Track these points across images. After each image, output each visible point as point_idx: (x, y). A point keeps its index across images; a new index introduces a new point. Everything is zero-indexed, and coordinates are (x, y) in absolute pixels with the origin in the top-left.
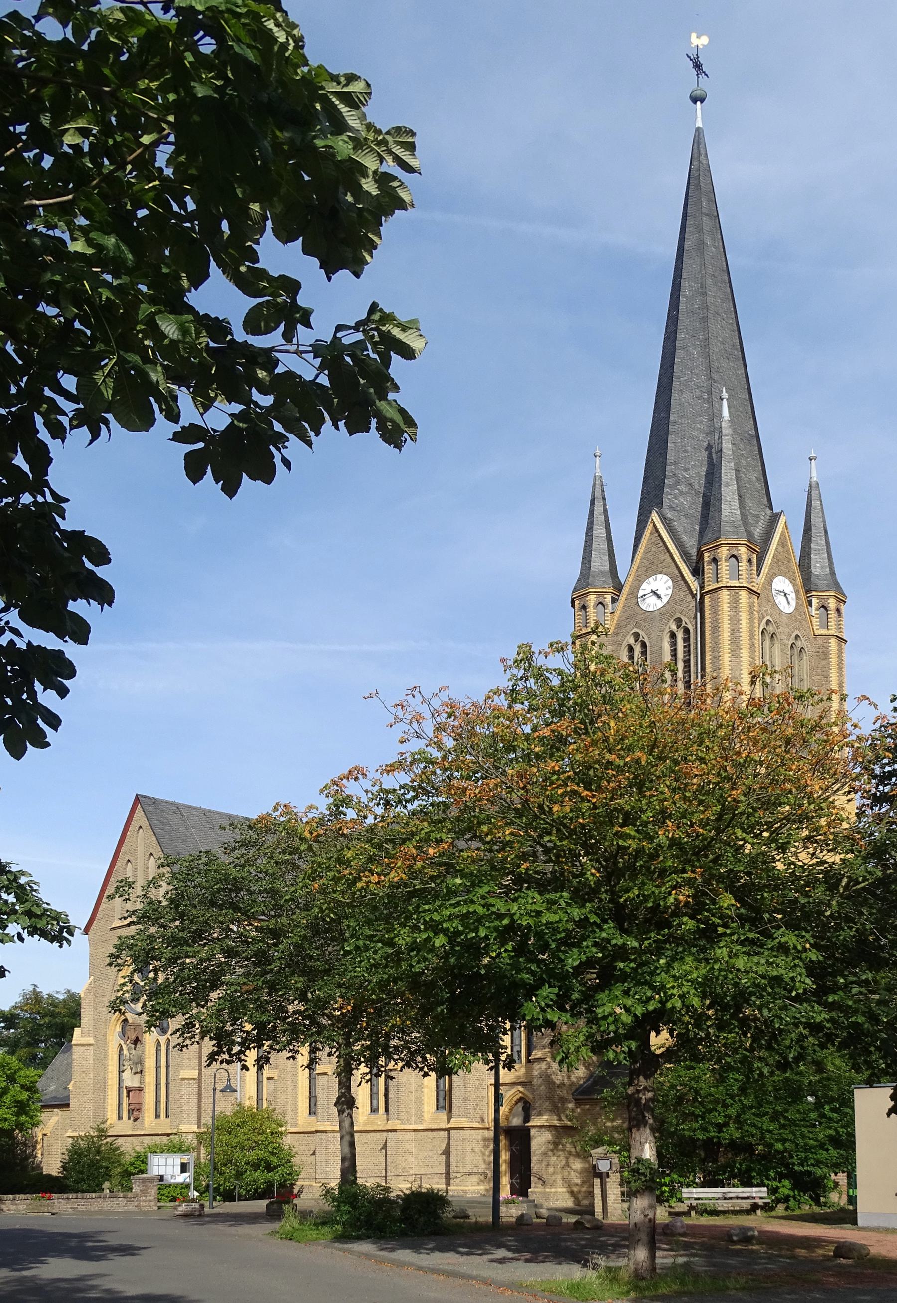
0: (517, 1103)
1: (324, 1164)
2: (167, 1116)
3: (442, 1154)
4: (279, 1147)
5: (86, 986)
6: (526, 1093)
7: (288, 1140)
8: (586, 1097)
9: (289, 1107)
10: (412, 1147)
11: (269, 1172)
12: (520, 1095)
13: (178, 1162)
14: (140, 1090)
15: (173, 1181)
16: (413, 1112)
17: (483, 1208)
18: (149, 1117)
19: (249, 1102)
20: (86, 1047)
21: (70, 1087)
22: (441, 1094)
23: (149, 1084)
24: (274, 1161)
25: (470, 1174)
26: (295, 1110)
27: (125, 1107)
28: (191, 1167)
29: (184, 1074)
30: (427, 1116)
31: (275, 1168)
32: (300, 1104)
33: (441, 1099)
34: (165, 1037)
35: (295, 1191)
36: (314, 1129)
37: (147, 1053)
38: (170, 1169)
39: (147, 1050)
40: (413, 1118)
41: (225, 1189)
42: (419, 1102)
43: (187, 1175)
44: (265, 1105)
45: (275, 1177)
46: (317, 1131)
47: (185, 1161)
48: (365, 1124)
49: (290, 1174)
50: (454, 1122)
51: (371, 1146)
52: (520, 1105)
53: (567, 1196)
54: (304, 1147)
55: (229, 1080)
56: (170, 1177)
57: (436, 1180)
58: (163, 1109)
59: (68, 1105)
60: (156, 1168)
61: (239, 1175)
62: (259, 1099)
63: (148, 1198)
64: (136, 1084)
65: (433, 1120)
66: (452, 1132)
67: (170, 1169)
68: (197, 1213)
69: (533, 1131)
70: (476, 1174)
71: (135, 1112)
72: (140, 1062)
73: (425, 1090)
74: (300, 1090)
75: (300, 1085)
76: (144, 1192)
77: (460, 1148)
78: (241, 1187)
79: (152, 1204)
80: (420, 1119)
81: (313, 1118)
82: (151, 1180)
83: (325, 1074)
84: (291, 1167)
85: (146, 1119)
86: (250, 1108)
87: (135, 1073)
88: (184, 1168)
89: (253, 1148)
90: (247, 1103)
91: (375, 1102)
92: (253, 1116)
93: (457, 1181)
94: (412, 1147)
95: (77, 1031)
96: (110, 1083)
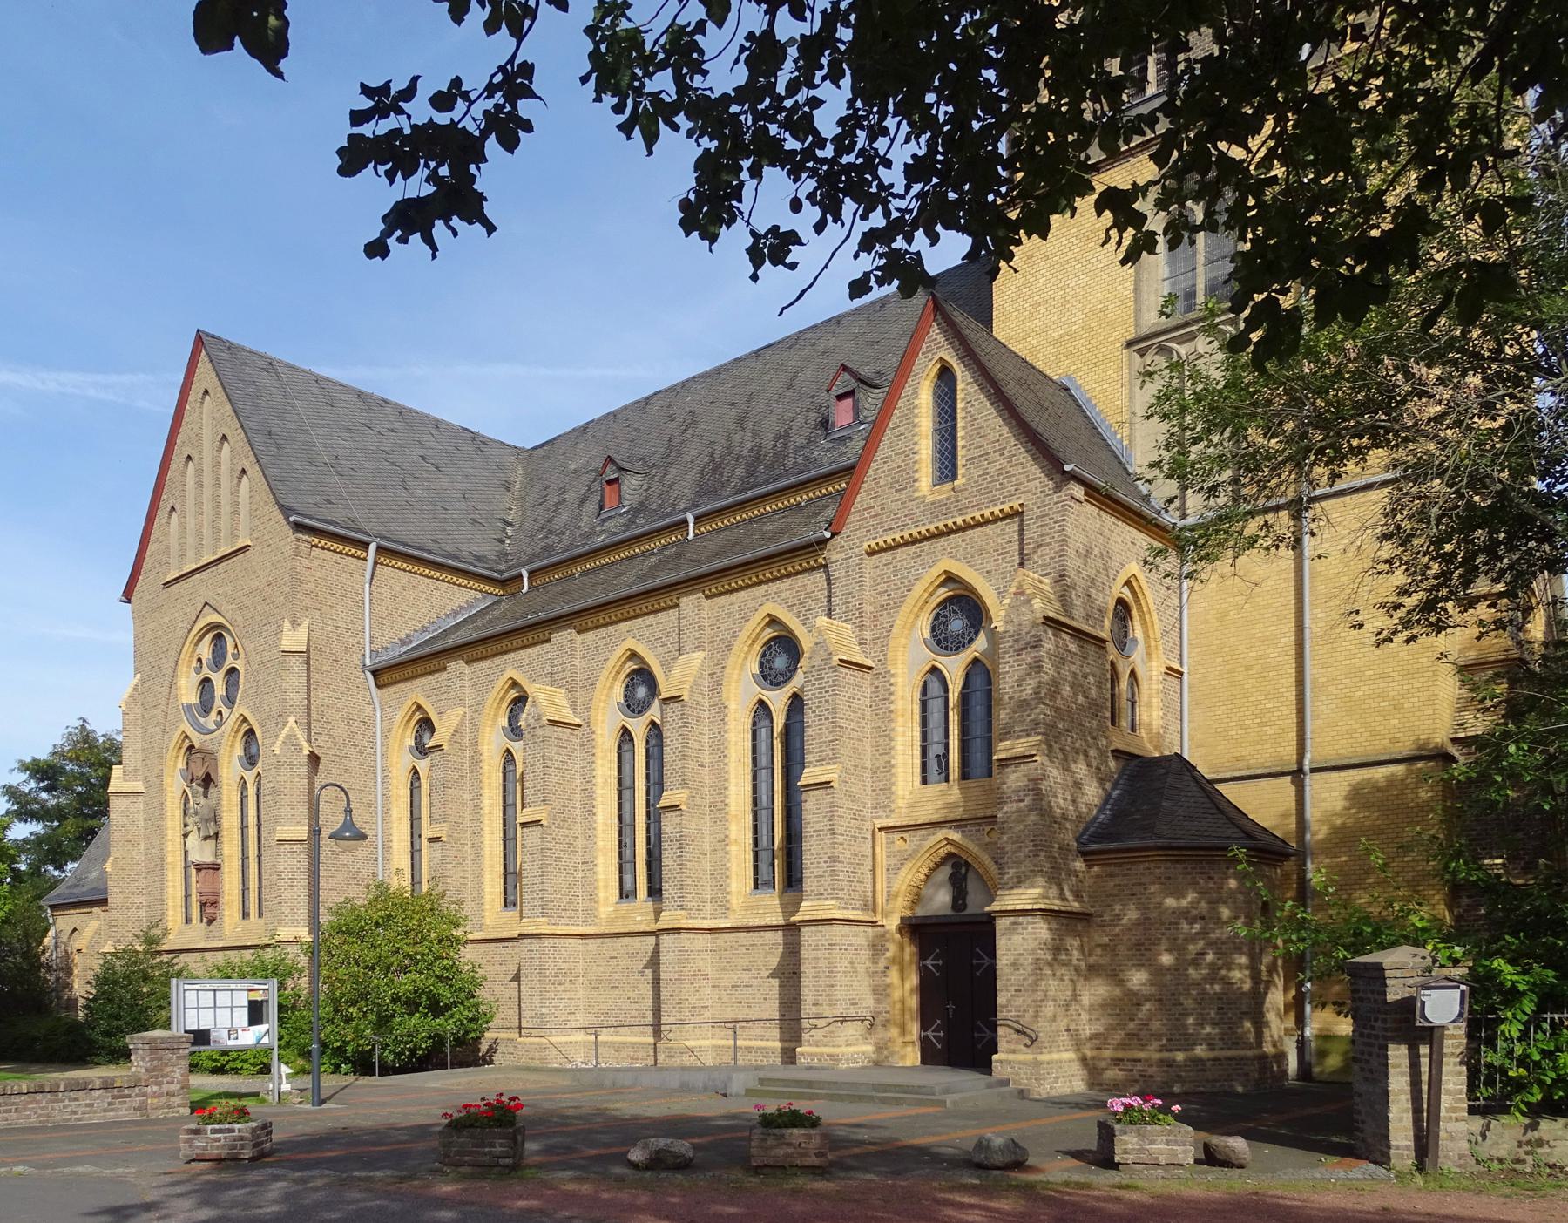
0: (938, 865)
1: (536, 999)
2: (260, 915)
3: (771, 976)
4: (454, 968)
5: (129, 690)
6: (972, 846)
7: (468, 954)
8: (1112, 846)
9: (467, 895)
10: (706, 963)
11: (435, 1017)
12: (948, 848)
13: (243, 999)
14: (216, 868)
15: (231, 1043)
16: (708, 894)
17: (919, 1103)
18: (231, 916)
19: (400, 882)
20: (132, 798)
21: (108, 867)
22: (765, 857)
23: (230, 856)
24: (446, 994)
25: (844, 1020)
26: (479, 900)
27: (194, 897)
28: (272, 1011)
29: (284, 832)
30: (736, 901)
31: (448, 1007)
32: (487, 888)
33: (764, 867)
34: (254, 772)
35: (484, 1047)
36: (515, 933)
37: (224, 802)
38: (223, 1014)
39: (225, 797)
40: (708, 907)
41: (355, 1052)
42: (721, 876)
43: (263, 1028)
44: (425, 887)
45: (447, 1025)
46: (523, 936)
47: (258, 996)
48: (612, 922)
49: (473, 1020)
50: (808, 909)
51: (623, 964)
52: (946, 871)
53: (1076, 1066)
54: (497, 967)
55: (349, 811)
56: (224, 1034)
57: (759, 1031)
58: (256, 903)
59: (103, 902)
60: (191, 1014)
61: (383, 1022)
62: (415, 881)
63: (165, 1088)
64: (208, 858)
65: (748, 909)
66: (806, 932)
67: (223, 1014)
68: (247, 1153)
69: (1002, 924)
70: (853, 1019)
71: (210, 905)
72: (215, 818)
73: (733, 849)
74: (487, 862)
75: (486, 852)
76: (156, 1074)
77: (823, 963)
78: (385, 1047)
79: (177, 1100)
80: (723, 907)
81: (513, 913)
82: (172, 1045)
83: (536, 823)
84: (476, 1005)
85: (226, 919)
86: (398, 894)
87: (206, 838)
88: (256, 1013)
89: (404, 970)
90: (395, 883)
91: (628, 878)
92: (403, 905)
93: (818, 1034)
94: (706, 963)
95: (117, 772)
96: (170, 859)
